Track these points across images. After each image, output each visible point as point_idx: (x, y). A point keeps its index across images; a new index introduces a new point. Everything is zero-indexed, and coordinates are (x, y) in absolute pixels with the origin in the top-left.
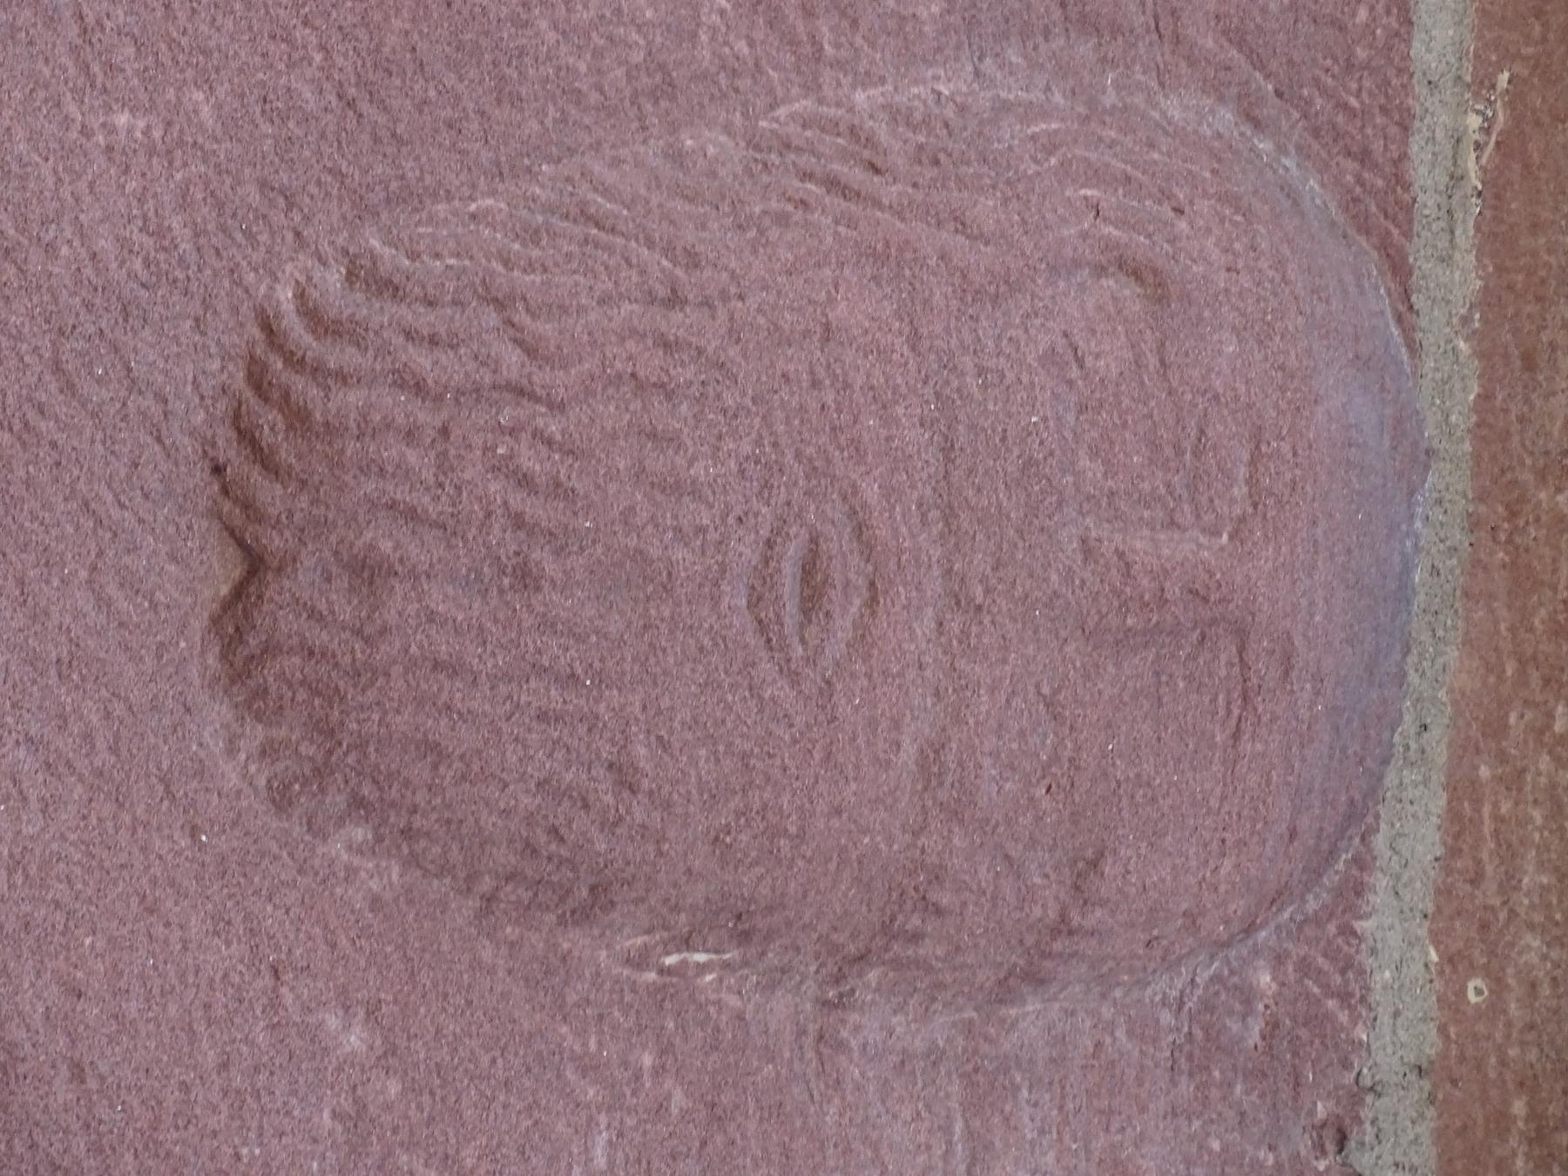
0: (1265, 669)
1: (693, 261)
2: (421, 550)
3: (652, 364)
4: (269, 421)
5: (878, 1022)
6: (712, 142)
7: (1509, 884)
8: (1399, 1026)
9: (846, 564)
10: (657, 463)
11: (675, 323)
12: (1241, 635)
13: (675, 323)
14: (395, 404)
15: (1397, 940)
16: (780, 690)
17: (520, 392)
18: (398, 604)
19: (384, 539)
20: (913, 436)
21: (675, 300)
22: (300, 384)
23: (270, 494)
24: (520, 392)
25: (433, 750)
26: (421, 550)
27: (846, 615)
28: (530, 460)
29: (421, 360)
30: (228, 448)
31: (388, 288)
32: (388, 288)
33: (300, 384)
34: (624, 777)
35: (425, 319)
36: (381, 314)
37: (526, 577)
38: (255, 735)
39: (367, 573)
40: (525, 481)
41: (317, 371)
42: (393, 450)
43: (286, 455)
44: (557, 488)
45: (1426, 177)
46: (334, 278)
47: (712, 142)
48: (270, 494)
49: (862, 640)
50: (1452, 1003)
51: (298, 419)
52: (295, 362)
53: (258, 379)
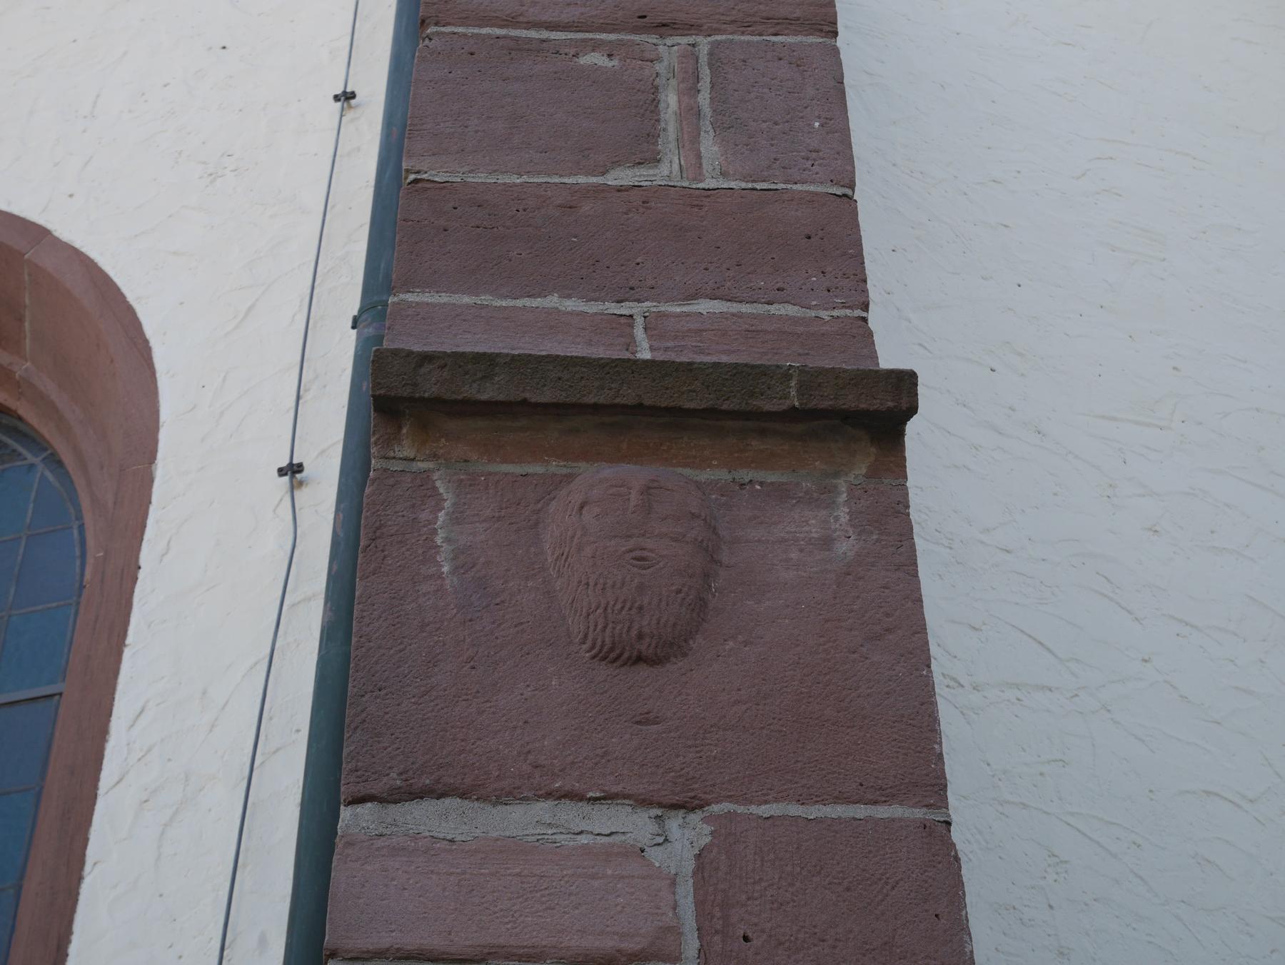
0: (656, 484)
1: (580, 582)
2: (636, 626)
3: (600, 587)
4: (613, 655)
5: (725, 557)
6: (558, 585)
7: (695, 457)
8: (723, 475)
9: (638, 553)
10: (618, 585)
11: (591, 584)
12: (649, 488)
13: (591, 584)
14: (608, 631)
15: (704, 476)
16: (661, 564)
17: (606, 609)
18: (646, 630)
19: (634, 633)
20: (613, 543)
21: (588, 584)
22: (605, 650)
23: (626, 655)
24: (606, 609)
25: (675, 625)
26: (636, 626)
27: (645, 554)
28: (618, 606)
29: (600, 627)
30: (617, 664)
31: (586, 636)
32: (586, 636)
33: (605, 650)
34: (679, 591)
35: (592, 628)
36: (591, 637)
37: (641, 608)
38: (673, 659)
39: (640, 636)
40: (623, 608)
41: (602, 646)
42: (617, 631)
43: (618, 652)
44: (624, 602)
45: (564, 471)
46: (584, 647)
47: (558, 585)
48: (626, 655)
49: (651, 551)
50: (717, 466)
51: (612, 649)
52: (600, 651)
53: (604, 659)
